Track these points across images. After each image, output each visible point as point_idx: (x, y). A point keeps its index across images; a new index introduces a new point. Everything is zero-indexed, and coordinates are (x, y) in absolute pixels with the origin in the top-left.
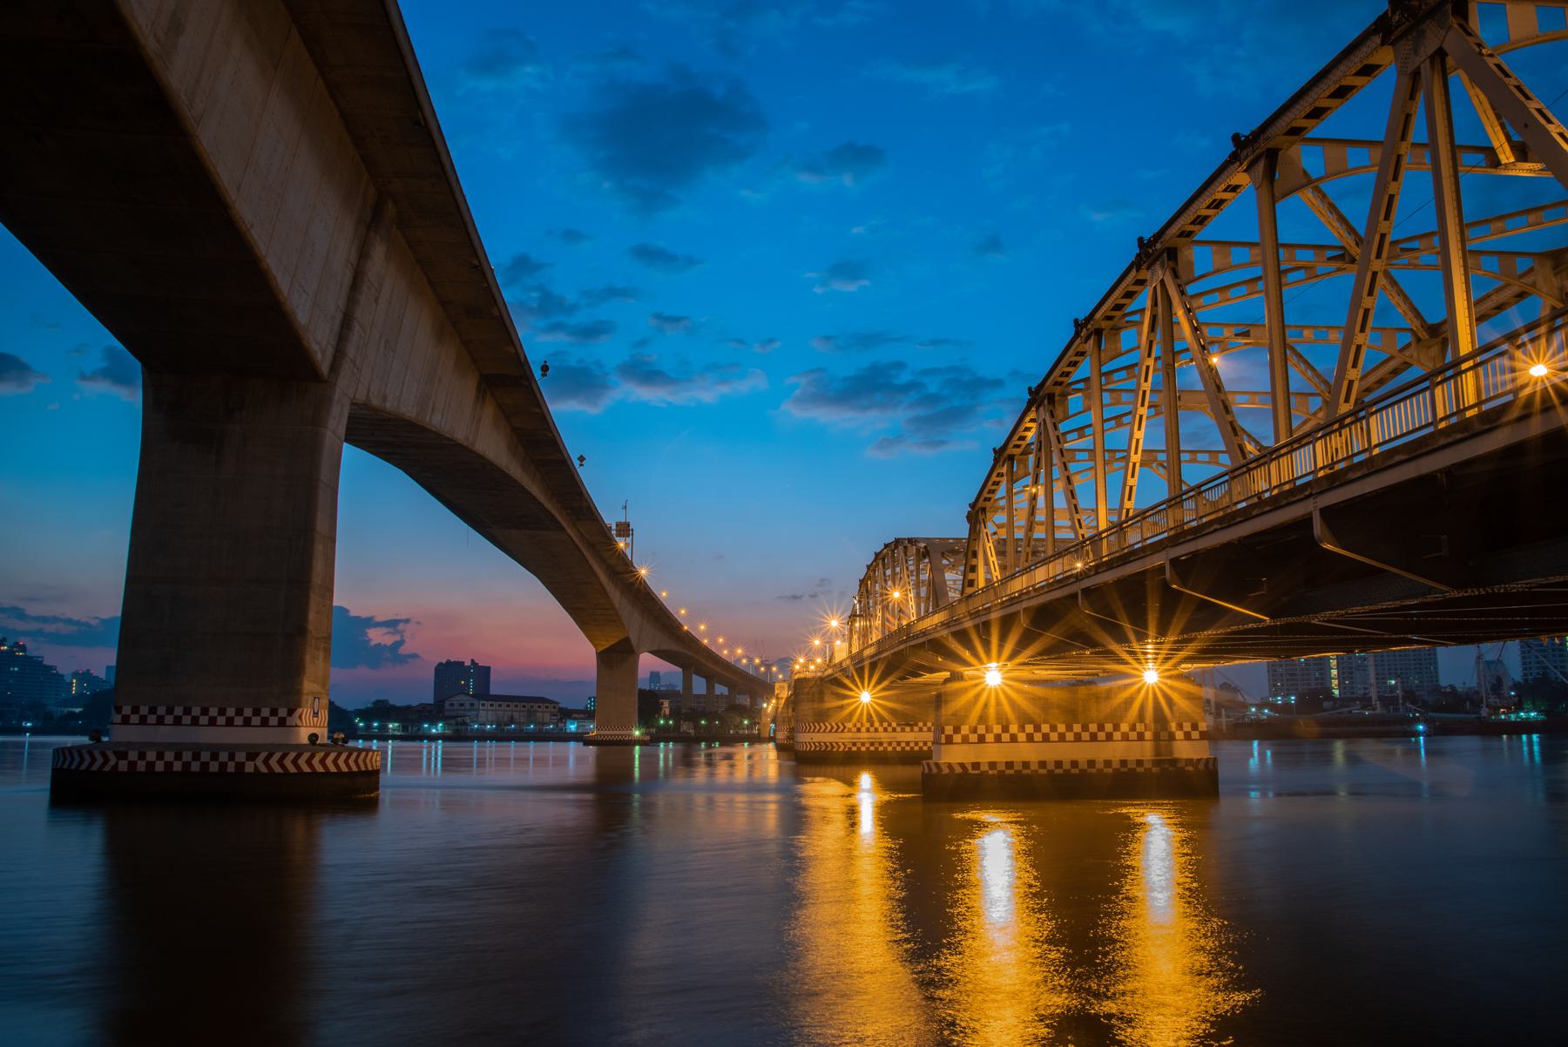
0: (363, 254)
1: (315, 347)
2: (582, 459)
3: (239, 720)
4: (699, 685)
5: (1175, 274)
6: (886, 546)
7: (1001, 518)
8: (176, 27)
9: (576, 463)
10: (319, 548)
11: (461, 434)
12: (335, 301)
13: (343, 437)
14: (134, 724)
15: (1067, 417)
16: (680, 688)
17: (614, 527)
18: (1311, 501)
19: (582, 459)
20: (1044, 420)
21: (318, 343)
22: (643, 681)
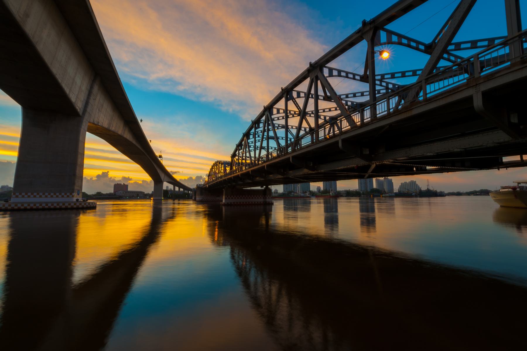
0: (91, 87)
1: (77, 108)
2: (150, 141)
4: (177, 189)
5: (270, 114)
7: (237, 157)
8: (27, 15)
11: (120, 132)
13: (86, 130)
14: (49, 197)
16: (173, 189)
17: (158, 156)
19: (150, 141)
20: (267, 114)
21: (78, 107)
22: (164, 188)
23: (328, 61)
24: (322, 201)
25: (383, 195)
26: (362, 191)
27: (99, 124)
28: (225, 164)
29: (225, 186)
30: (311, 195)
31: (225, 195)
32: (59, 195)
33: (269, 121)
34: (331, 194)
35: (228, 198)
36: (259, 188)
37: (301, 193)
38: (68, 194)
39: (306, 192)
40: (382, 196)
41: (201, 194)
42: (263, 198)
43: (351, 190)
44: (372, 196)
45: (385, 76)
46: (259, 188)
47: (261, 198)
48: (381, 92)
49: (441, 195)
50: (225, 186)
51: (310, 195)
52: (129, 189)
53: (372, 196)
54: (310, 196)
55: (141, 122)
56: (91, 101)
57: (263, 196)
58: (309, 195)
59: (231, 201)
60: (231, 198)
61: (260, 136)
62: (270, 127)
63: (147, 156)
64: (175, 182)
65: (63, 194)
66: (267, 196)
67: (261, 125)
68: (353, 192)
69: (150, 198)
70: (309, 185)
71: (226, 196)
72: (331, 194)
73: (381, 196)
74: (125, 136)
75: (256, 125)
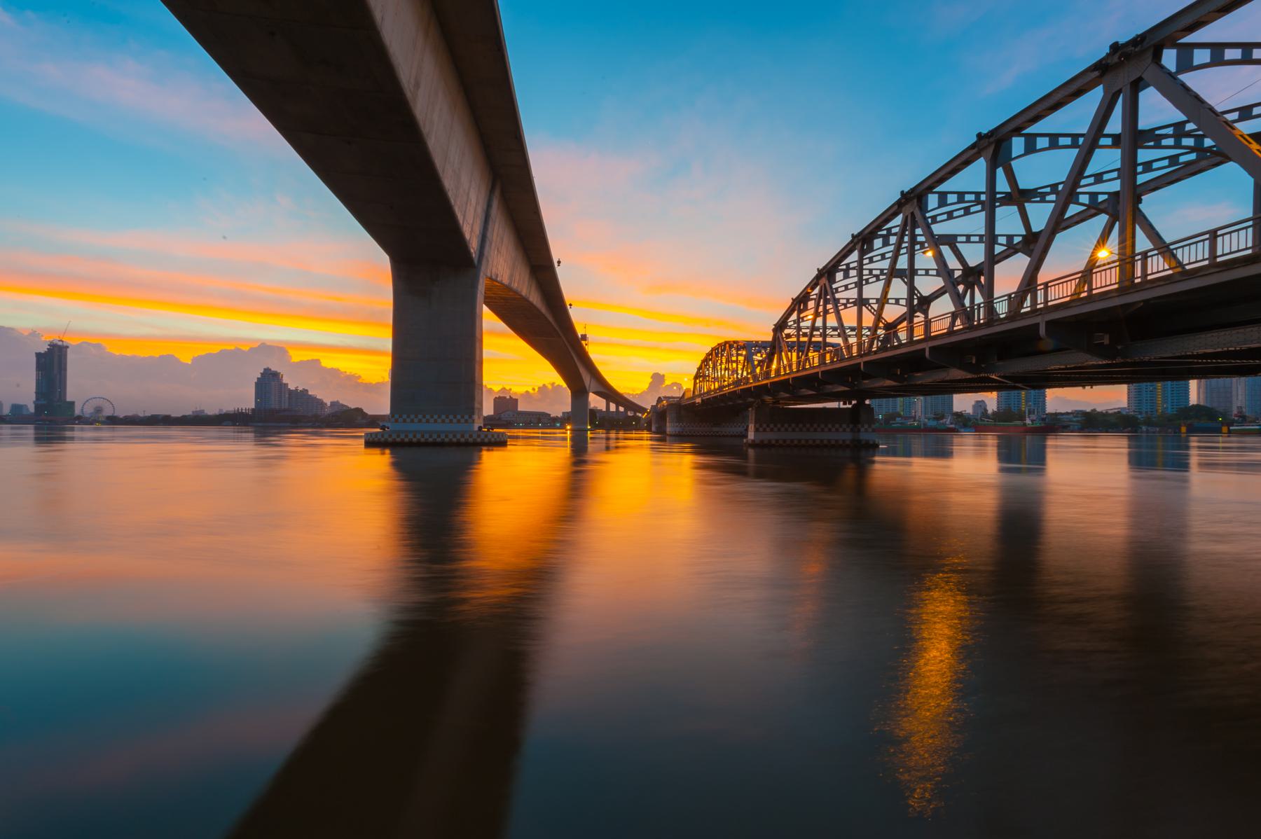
0: (489, 206)
1: (472, 251)
3: (424, 420)
4: (613, 407)
5: (920, 209)
6: (718, 344)
8: (417, 85)
9: (569, 307)
10: (477, 345)
12: (478, 229)
15: (835, 282)
16: (604, 409)
18: (1040, 317)
19: (571, 305)
20: (825, 284)
23: (941, 181)
24: (991, 441)
25: (1231, 428)
26: (1141, 413)
27: (498, 279)
28: (749, 347)
29: (751, 400)
30: (961, 424)
31: (756, 423)
33: (826, 294)
34: (1028, 421)
35: (761, 429)
37: (929, 420)
39: (943, 417)
40: (1229, 432)
41: (679, 419)
42: (852, 430)
43: (1099, 409)
44: (1184, 429)
45: (1093, 181)
47: (844, 430)
48: (1183, 159)
50: (751, 400)
51: (956, 424)
52: (520, 408)
53: (1184, 429)
54: (957, 427)
55: (559, 265)
56: (489, 235)
57: (851, 426)
58: (951, 424)
59: (770, 436)
60: (768, 429)
62: (829, 306)
63: (563, 337)
64: (608, 393)
66: (863, 426)
67: (811, 304)
68: (1105, 415)
69: (562, 427)
70: (952, 397)
71: (758, 426)
72: (1028, 421)
73: (1225, 429)
74: (531, 299)
75: (800, 306)
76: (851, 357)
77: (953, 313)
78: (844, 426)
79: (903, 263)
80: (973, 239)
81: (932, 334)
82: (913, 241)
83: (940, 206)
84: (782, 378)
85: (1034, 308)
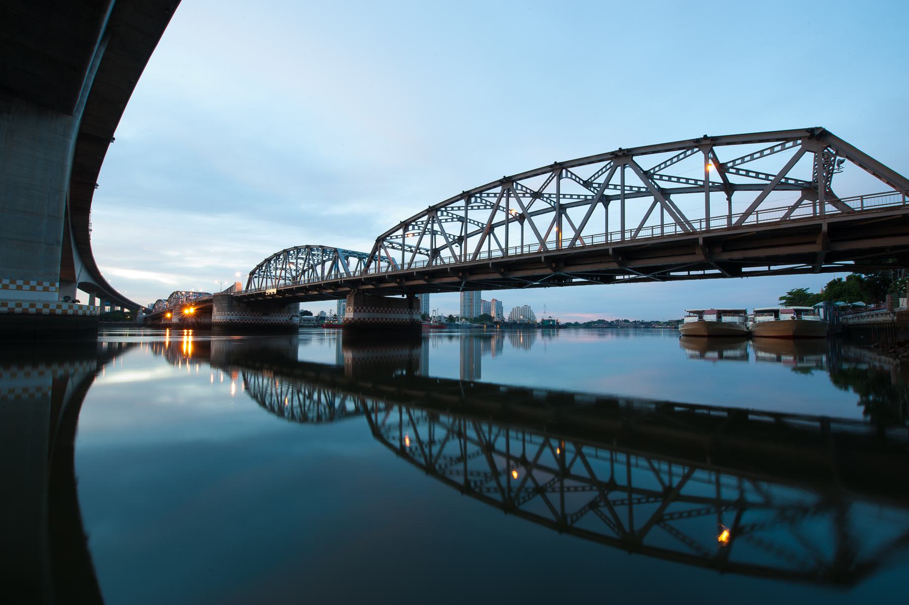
32: (11, 283)
35: (358, 311)
36: (400, 296)
38: (46, 284)
46: (400, 296)
49: (589, 326)
57: (409, 310)
61: (421, 228)
65: (33, 283)
66: (414, 311)
71: (355, 308)
76: (319, 282)
77: (675, 223)
78: (405, 310)
79: (284, 267)
80: (664, 178)
81: (711, 228)
82: (286, 262)
83: (475, 202)
84: (301, 286)
85: (729, 226)
